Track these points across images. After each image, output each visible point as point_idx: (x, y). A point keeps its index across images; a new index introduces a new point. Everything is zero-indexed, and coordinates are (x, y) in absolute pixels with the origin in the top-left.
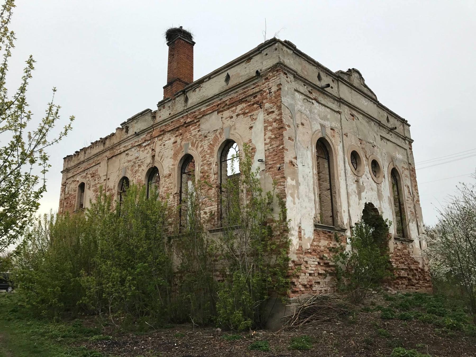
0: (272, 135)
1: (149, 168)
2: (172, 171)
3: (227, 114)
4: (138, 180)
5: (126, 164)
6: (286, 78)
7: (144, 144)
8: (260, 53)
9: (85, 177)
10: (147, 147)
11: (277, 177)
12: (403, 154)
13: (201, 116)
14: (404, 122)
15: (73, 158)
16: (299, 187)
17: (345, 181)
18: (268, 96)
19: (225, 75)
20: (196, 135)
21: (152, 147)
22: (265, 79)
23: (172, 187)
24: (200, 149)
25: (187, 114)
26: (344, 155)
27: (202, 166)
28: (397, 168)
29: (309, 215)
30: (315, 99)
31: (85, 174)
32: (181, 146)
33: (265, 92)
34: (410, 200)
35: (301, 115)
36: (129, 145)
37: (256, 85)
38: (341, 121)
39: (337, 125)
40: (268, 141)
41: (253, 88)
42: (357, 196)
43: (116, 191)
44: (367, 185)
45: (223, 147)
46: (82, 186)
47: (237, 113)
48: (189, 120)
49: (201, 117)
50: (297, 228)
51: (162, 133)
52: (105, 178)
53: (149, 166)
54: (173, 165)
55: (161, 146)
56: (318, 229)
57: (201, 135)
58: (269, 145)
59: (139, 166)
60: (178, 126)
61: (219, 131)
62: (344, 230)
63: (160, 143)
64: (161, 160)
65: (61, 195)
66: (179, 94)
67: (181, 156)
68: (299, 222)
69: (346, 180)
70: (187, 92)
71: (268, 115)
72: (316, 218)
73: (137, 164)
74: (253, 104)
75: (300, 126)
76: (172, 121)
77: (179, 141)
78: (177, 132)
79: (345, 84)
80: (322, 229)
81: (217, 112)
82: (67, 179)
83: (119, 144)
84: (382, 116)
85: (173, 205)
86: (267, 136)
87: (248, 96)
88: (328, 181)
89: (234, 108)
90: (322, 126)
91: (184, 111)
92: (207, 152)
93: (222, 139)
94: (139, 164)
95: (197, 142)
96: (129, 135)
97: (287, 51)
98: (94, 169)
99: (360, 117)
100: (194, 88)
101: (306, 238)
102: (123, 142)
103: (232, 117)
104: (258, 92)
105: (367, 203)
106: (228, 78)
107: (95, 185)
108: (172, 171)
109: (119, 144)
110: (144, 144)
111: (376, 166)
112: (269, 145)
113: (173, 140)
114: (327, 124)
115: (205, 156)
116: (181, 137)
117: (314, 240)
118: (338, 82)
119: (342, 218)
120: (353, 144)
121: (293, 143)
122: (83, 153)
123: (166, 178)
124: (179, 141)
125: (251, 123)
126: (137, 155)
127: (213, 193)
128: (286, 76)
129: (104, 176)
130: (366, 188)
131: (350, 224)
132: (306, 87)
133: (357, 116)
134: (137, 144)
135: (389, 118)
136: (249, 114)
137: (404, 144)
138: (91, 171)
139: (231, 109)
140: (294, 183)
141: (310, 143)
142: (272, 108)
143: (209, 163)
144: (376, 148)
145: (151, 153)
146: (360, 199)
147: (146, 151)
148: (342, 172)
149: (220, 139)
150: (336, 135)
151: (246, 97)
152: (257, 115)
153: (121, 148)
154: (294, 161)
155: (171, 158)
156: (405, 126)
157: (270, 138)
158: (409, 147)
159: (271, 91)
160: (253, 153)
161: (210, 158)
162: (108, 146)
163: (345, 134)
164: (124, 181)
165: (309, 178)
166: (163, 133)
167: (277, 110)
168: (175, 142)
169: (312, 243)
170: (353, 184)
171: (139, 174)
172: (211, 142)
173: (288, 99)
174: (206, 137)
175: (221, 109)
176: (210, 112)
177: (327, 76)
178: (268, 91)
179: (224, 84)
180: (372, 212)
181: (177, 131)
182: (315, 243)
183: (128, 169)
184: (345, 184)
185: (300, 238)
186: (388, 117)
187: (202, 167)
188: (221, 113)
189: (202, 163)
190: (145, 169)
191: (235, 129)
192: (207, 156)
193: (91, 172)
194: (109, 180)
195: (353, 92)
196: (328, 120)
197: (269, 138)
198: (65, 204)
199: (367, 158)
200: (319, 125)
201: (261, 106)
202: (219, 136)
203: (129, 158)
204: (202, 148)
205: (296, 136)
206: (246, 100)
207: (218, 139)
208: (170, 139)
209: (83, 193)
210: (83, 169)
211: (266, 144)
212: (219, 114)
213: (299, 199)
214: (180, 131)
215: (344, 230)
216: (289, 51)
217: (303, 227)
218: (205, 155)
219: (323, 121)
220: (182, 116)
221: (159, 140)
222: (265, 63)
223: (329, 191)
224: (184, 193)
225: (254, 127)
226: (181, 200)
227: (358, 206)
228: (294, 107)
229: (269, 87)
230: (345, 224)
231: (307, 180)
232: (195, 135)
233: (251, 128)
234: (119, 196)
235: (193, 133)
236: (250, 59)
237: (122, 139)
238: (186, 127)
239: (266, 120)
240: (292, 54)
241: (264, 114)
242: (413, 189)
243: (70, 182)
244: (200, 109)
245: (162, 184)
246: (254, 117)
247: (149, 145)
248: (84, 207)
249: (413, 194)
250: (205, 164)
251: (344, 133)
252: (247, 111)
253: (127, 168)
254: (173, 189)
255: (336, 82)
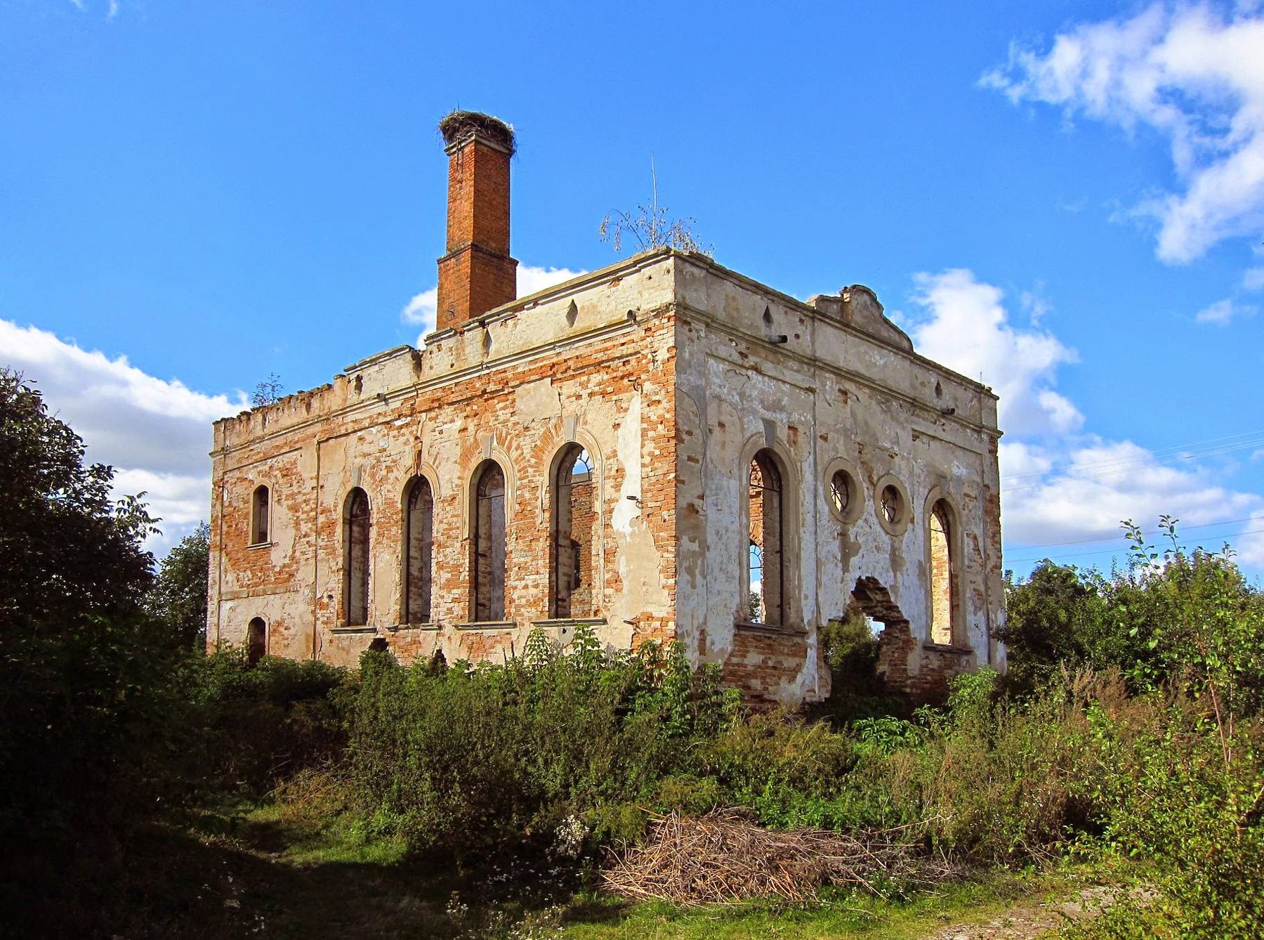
0: (655, 448)
1: (409, 476)
2: (458, 490)
3: (569, 387)
4: (386, 499)
5: (360, 461)
6: (688, 333)
7: (398, 423)
8: (638, 271)
9: (267, 475)
10: (403, 430)
11: (662, 534)
12: (968, 466)
13: (518, 382)
14: (982, 392)
15: (237, 426)
16: (707, 553)
17: (813, 536)
18: (651, 366)
19: (568, 301)
20: (508, 420)
21: (415, 432)
22: (646, 330)
23: (458, 525)
24: (514, 454)
25: (487, 371)
26: (816, 480)
27: (519, 489)
28: (949, 500)
29: (725, 606)
30: (756, 369)
31: (267, 468)
32: (476, 440)
33: (645, 357)
34: (976, 567)
35: (719, 406)
36: (365, 418)
37: (629, 338)
38: (814, 409)
39: (805, 417)
40: (647, 460)
41: (623, 344)
42: (840, 565)
43: (338, 515)
44: (867, 540)
45: (562, 455)
46: (262, 493)
47: (589, 391)
48: (492, 387)
49: (518, 386)
50: (697, 634)
51: (436, 405)
52: (314, 483)
53: (409, 473)
54: (459, 478)
55: (434, 434)
56: (742, 632)
57: (518, 423)
58: (649, 469)
59: (389, 469)
60: (469, 395)
61: (553, 421)
62: (803, 634)
63: (431, 424)
64: (434, 463)
65: (214, 506)
66: (472, 325)
67: (475, 462)
68: (701, 620)
69: (816, 533)
70: (488, 324)
71: (648, 406)
72: (741, 612)
73: (384, 465)
74: (622, 378)
75: (717, 430)
76: (456, 381)
77: (471, 428)
78: (468, 409)
79: (830, 324)
80: (752, 633)
81: (550, 379)
82: (225, 473)
83: (344, 412)
84: (923, 384)
85: (462, 561)
86: (646, 450)
87: (613, 359)
88: (778, 535)
89: (584, 378)
90: (770, 425)
91: (482, 365)
92: (529, 461)
93: (561, 441)
94: (388, 463)
95: (509, 437)
96: (363, 397)
97: (692, 274)
98: (287, 458)
99: (863, 394)
100: (502, 318)
101: (715, 650)
102: (351, 411)
103: (579, 397)
104: (631, 355)
105: (863, 578)
106: (573, 311)
107: (292, 496)
108: (458, 490)
109: (344, 412)
110: (398, 423)
111: (896, 497)
112: (649, 469)
113: (459, 423)
114: (781, 418)
115: (524, 469)
116: (476, 422)
117: (731, 655)
118: (813, 321)
119: (799, 611)
120: (839, 455)
121: (698, 466)
122: (260, 417)
123: (446, 504)
124: (471, 428)
125: (618, 418)
126: (382, 444)
127: (541, 548)
128: (687, 328)
129: (311, 479)
130: (863, 546)
131: (817, 621)
132: (734, 344)
133: (857, 392)
134: (381, 420)
135: (942, 386)
136: (614, 398)
137: (976, 443)
138: (280, 462)
139: (578, 380)
140: (695, 547)
141: (736, 461)
142: (656, 394)
143: (533, 485)
144: (896, 459)
145: (413, 444)
146: (846, 569)
147: (402, 439)
148: (809, 518)
149: (556, 439)
150: (801, 439)
151: (608, 361)
152: (629, 401)
153: (347, 423)
154: (697, 502)
155: (456, 462)
156: (986, 400)
157: (651, 454)
158: (990, 447)
159: (657, 358)
160: (619, 480)
161: (534, 476)
162: (317, 412)
163: (821, 437)
164: (357, 498)
165: (729, 534)
166: (438, 404)
167: (666, 401)
168: (465, 430)
169: (729, 659)
170: (832, 540)
171: (390, 487)
172: (538, 443)
173: (690, 377)
174: (527, 428)
175: (559, 376)
176: (537, 377)
177: (786, 313)
178: (650, 356)
179: (565, 321)
180: (877, 594)
181: (468, 405)
182: (735, 660)
183: (365, 471)
184: (812, 541)
185: (702, 650)
186: (938, 384)
187: (519, 492)
188: (559, 385)
189: (519, 483)
190: (401, 478)
191: (585, 423)
192: (531, 470)
193: (281, 465)
194: (324, 490)
195: (850, 338)
196: (782, 409)
197: (649, 455)
198: (225, 528)
199: (873, 483)
200: (761, 422)
201: (637, 385)
202: (553, 431)
203: (366, 448)
204: (519, 452)
205: (705, 451)
206: (609, 367)
207: (553, 437)
208: (452, 421)
209: (263, 509)
210: (262, 455)
211: (643, 465)
212: (555, 385)
213: (705, 578)
214: (475, 407)
215: (803, 634)
216: (696, 271)
217: (708, 629)
218: (526, 467)
219: (770, 413)
220: (478, 374)
221: (431, 419)
222: (647, 296)
223: (779, 555)
224: (484, 539)
225: (622, 426)
226: (477, 553)
227: (840, 586)
228: (704, 391)
229: (653, 350)
230: (806, 621)
231: (725, 538)
232: (505, 422)
233: (616, 426)
234: (347, 527)
235: (503, 416)
236: (619, 279)
237: (349, 403)
238: (486, 400)
239: (646, 416)
240: (705, 277)
241: (642, 403)
242: (989, 541)
243: (234, 481)
244: (514, 367)
245: (438, 514)
246: (624, 405)
247: (407, 425)
248: (269, 540)
249: (985, 552)
250: (525, 487)
251: (819, 434)
252: (609, 389)
253: (361, 469)
254: (461, 528)
255: (808, 322)
